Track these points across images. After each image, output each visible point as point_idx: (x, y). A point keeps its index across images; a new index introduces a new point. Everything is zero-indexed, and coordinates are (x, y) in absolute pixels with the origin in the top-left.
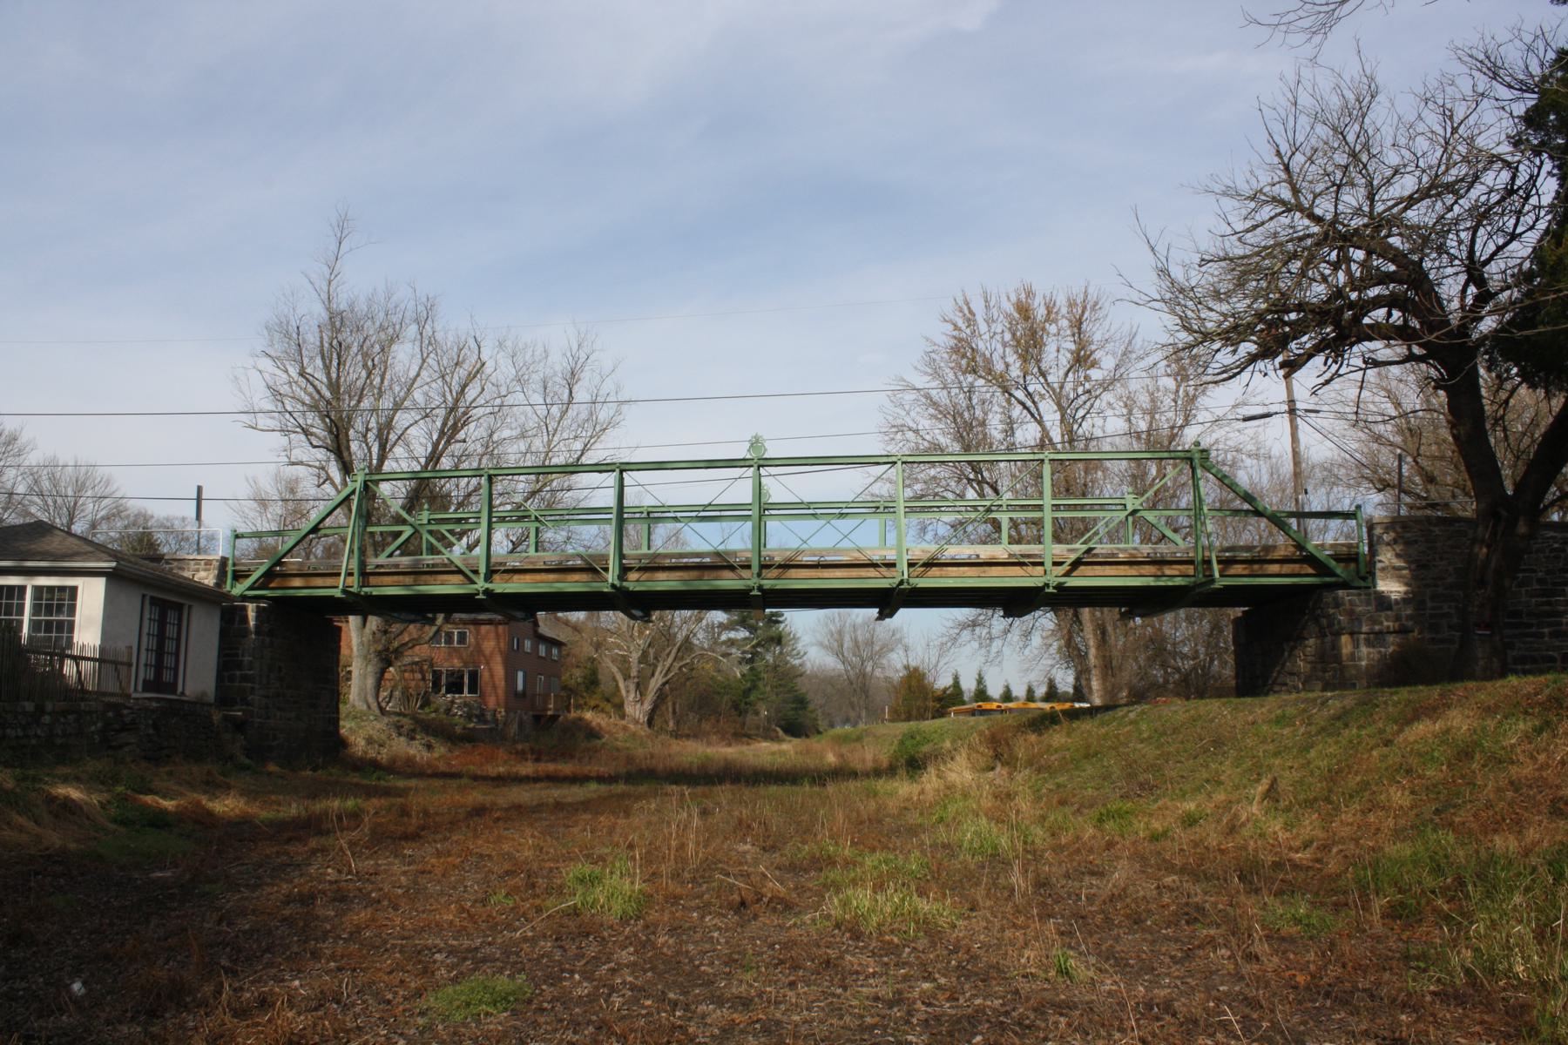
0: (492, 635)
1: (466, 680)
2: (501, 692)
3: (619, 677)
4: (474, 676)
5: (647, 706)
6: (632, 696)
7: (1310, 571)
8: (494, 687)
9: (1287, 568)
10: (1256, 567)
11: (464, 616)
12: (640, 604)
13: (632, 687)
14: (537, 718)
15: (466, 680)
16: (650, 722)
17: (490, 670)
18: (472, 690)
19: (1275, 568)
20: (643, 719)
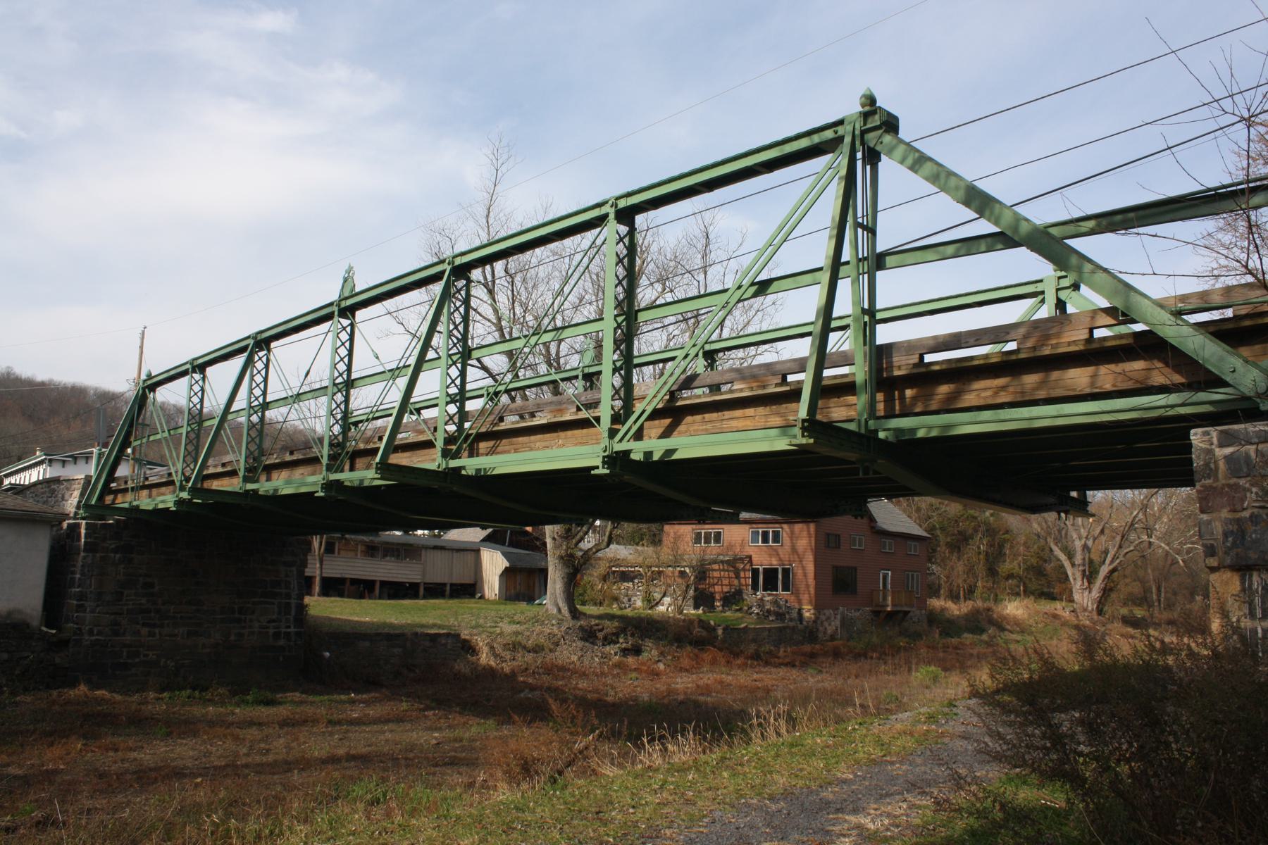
0: (805, 533)
1: (780, 576)
2: (812, 590)
3: (1067, 564)
4: (786, 572)
5: (1096, 593)
6: (1079, 583)
7: (1178, 379)
8: (807, 586)
9: (1107, 376)
10: (1031, 379)
11: (754, 516)
12: (519, 507)
13: (1079, 576)
14: (876, 613)
15: (780, 576)
16: (1100, 612)
17: (804, 568)
18: (786, 588)
19: (1078, 377)
20: (1092, 606)
